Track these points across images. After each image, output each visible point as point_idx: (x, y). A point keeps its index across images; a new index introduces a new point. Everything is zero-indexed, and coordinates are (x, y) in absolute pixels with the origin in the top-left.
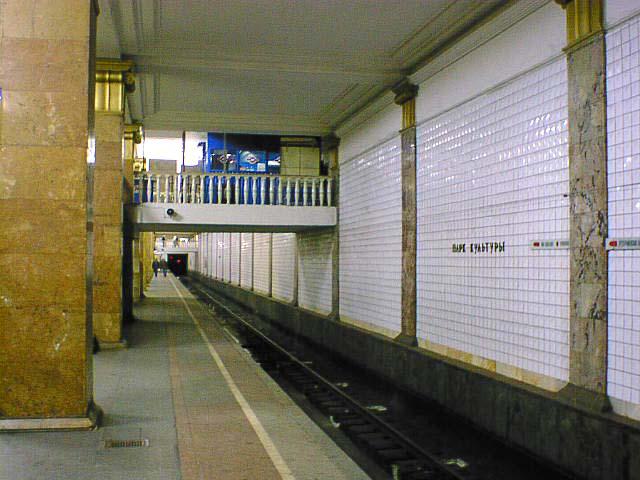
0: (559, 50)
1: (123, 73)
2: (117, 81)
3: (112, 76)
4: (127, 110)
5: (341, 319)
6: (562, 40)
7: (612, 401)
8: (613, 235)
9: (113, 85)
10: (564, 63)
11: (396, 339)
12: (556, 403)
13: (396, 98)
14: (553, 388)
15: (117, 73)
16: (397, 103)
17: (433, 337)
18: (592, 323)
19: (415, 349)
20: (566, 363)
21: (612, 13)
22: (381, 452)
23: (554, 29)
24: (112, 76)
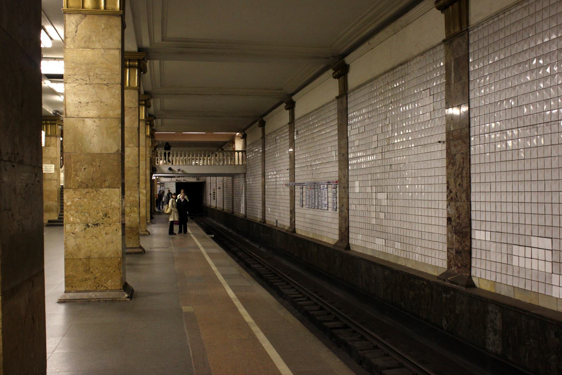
0: (334, 97)
1: (139, 61)
2: (134, 67)
3: (131, 63)
4: (128, 8)
5: (267, 223)
6: (441, 34)
7: (351, 246)
8: (296, 181)
9: (132, 70)
10: (288, 126)
11: (335, 245)
12: (437, 284)
13: (333, 74)
14: (332, 242)
15: (134, 60)
16: (335, 78)
17: (362, 242)
18: (460, 229)
19: (264, 224)
20: (444, 256)
21: (478, 10)
22: (326, 324)
23: (430, 25)
24: (131, 63)
